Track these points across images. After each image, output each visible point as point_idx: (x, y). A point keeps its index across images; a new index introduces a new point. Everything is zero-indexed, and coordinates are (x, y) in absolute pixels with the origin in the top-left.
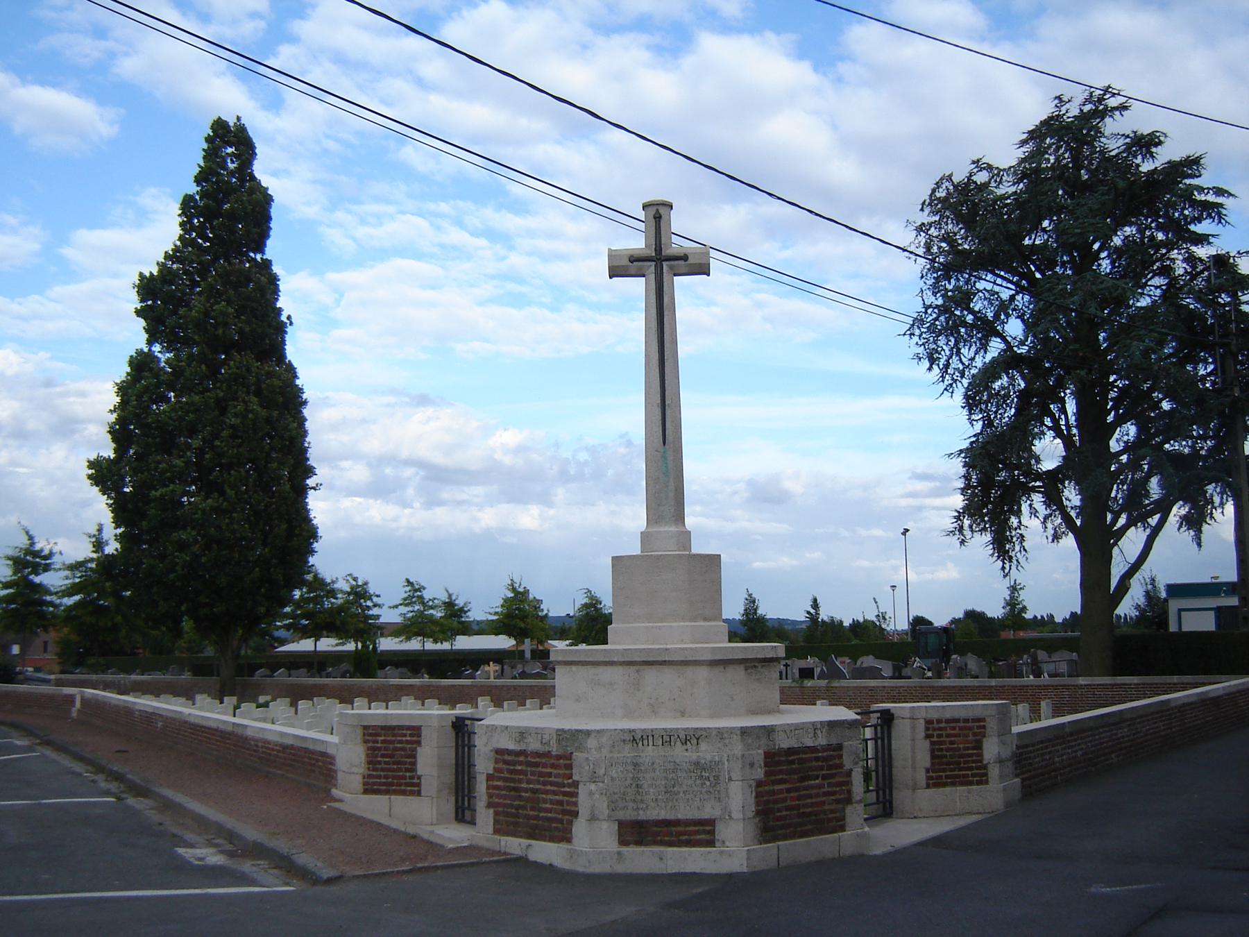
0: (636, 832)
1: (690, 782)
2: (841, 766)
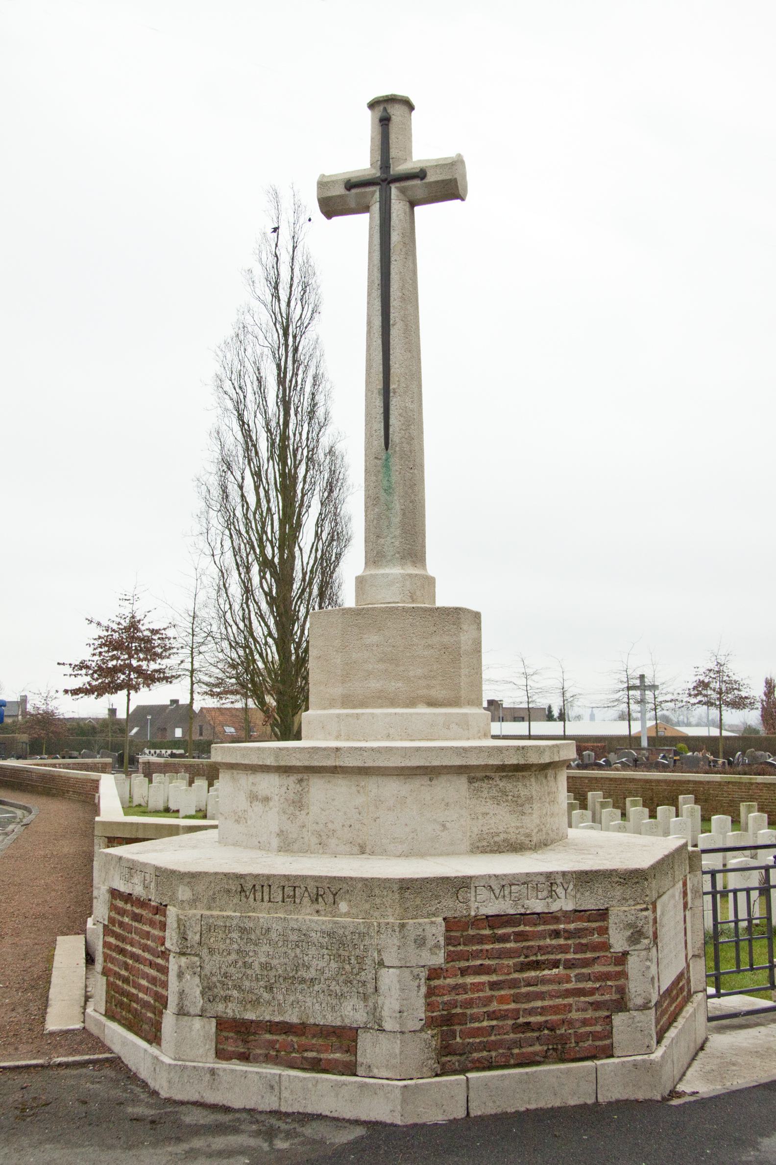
0: (238, 1038)
1: (321, 964)
2: (605, 946)
